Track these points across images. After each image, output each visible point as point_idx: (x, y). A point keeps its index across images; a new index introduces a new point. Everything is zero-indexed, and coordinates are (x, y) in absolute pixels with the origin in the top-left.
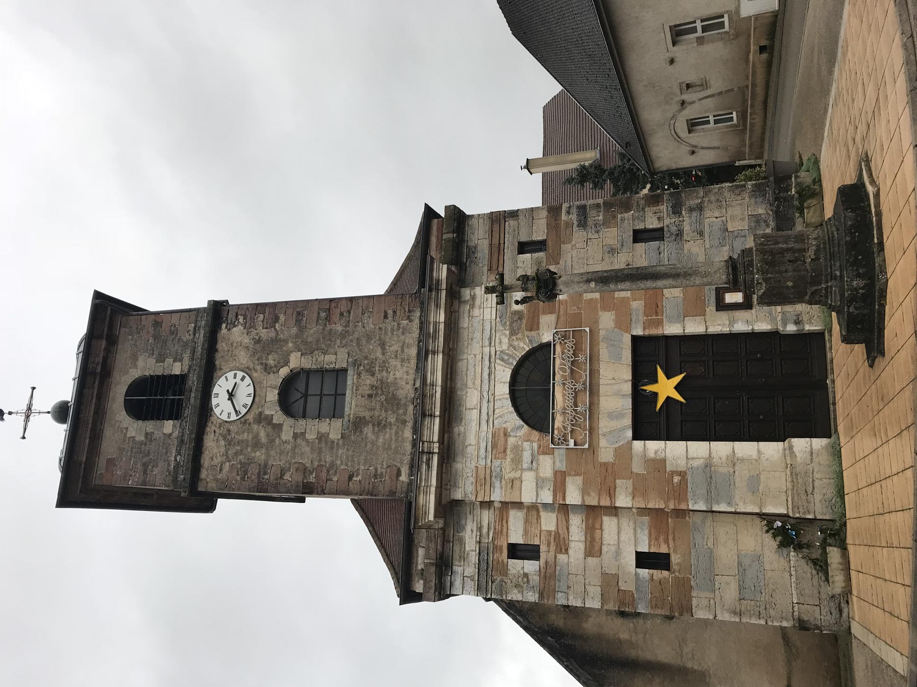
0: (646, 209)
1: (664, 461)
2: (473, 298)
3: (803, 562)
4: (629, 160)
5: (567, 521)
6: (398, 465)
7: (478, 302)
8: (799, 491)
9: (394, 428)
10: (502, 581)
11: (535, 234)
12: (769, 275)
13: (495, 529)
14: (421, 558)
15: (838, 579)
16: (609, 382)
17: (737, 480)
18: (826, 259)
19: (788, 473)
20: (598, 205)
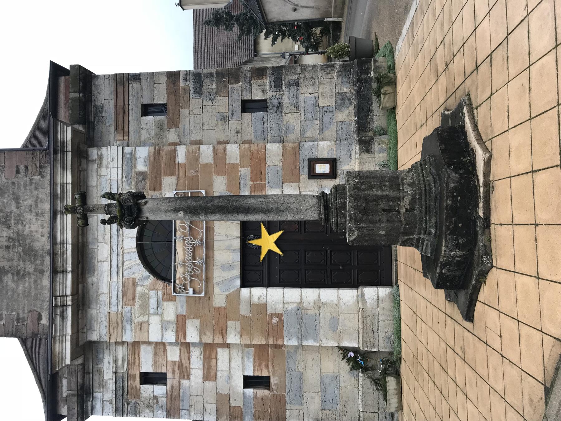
0: (253, 81)
1: (265, 306)
2: (100, 157)
3: (368, 381)
4: (250, 11)
5: (189, 353)
6: (39, 310)
7: (105, 162)
8: (368, 330)
9: (33, 277)
10: (136, 403)
11: (156, 98)
12: (363, 225)
13: (129, 361)
14: (65, 388)
15: (393, 401)
16: (222, 238)
17: (321, 321)
18: (421, 212)
19: (360, 315)
20: (211, 75)
